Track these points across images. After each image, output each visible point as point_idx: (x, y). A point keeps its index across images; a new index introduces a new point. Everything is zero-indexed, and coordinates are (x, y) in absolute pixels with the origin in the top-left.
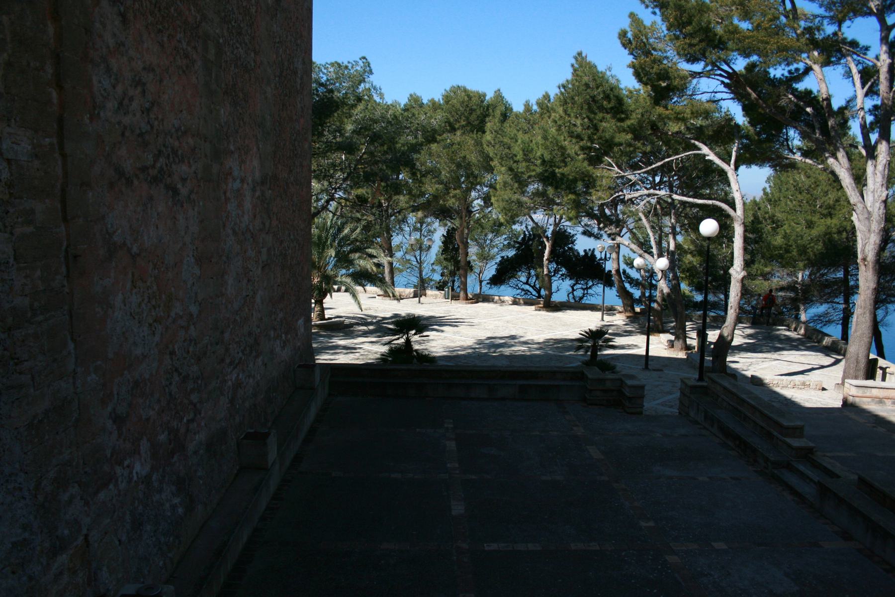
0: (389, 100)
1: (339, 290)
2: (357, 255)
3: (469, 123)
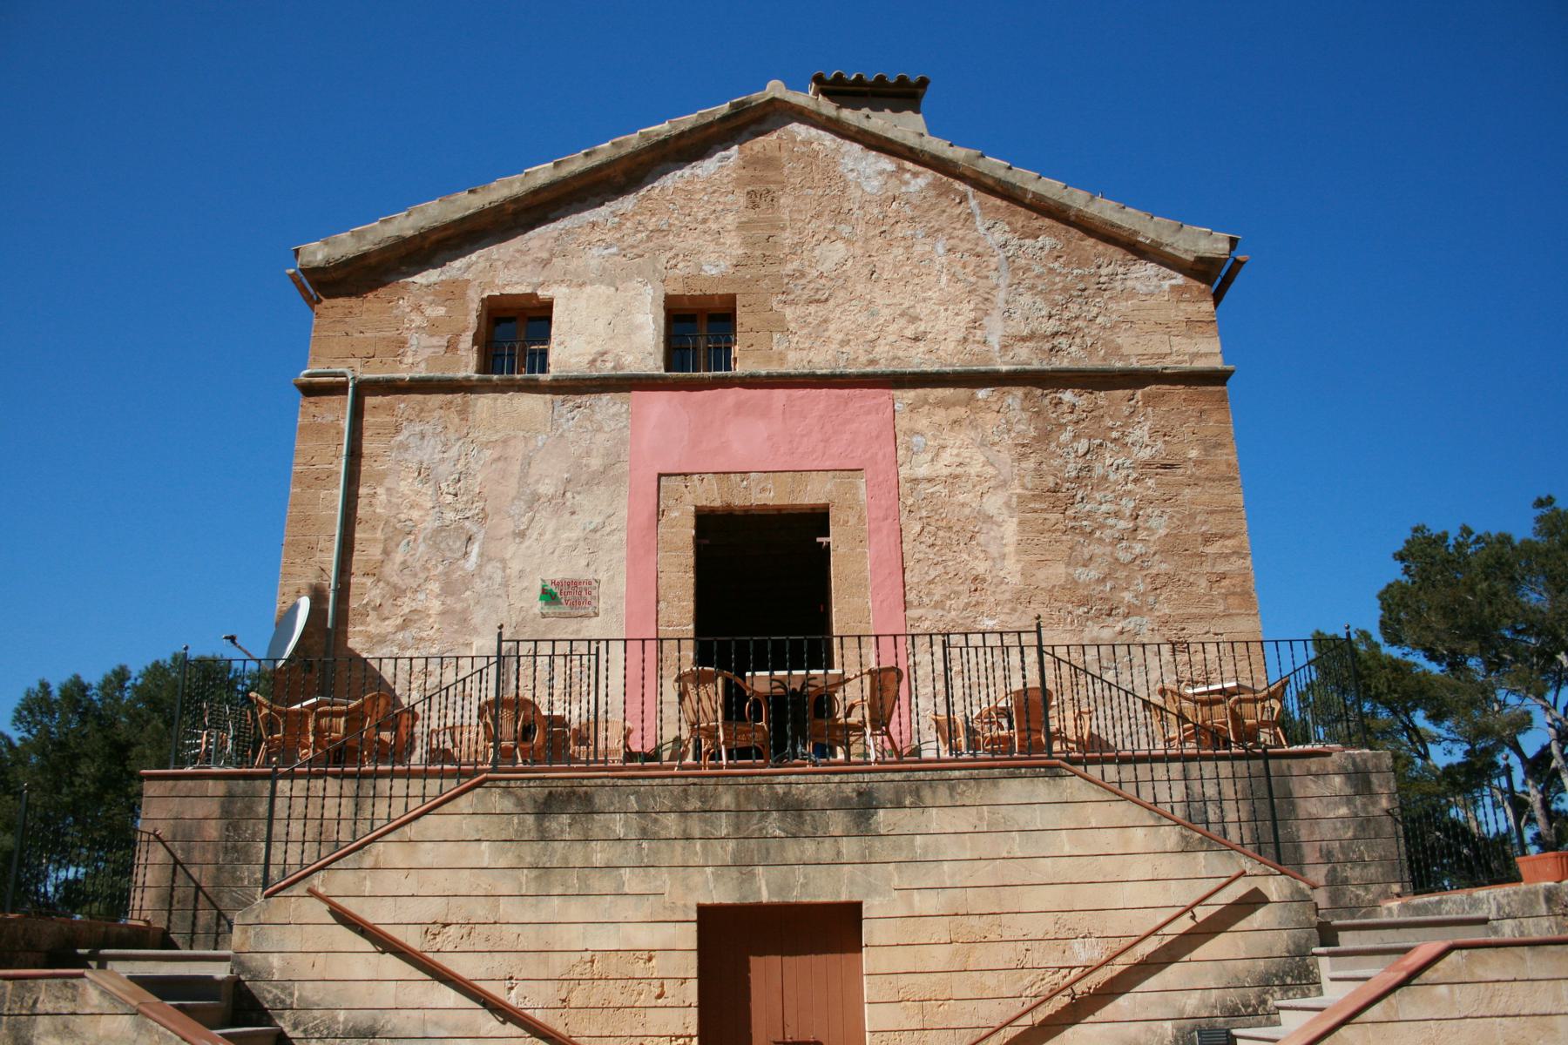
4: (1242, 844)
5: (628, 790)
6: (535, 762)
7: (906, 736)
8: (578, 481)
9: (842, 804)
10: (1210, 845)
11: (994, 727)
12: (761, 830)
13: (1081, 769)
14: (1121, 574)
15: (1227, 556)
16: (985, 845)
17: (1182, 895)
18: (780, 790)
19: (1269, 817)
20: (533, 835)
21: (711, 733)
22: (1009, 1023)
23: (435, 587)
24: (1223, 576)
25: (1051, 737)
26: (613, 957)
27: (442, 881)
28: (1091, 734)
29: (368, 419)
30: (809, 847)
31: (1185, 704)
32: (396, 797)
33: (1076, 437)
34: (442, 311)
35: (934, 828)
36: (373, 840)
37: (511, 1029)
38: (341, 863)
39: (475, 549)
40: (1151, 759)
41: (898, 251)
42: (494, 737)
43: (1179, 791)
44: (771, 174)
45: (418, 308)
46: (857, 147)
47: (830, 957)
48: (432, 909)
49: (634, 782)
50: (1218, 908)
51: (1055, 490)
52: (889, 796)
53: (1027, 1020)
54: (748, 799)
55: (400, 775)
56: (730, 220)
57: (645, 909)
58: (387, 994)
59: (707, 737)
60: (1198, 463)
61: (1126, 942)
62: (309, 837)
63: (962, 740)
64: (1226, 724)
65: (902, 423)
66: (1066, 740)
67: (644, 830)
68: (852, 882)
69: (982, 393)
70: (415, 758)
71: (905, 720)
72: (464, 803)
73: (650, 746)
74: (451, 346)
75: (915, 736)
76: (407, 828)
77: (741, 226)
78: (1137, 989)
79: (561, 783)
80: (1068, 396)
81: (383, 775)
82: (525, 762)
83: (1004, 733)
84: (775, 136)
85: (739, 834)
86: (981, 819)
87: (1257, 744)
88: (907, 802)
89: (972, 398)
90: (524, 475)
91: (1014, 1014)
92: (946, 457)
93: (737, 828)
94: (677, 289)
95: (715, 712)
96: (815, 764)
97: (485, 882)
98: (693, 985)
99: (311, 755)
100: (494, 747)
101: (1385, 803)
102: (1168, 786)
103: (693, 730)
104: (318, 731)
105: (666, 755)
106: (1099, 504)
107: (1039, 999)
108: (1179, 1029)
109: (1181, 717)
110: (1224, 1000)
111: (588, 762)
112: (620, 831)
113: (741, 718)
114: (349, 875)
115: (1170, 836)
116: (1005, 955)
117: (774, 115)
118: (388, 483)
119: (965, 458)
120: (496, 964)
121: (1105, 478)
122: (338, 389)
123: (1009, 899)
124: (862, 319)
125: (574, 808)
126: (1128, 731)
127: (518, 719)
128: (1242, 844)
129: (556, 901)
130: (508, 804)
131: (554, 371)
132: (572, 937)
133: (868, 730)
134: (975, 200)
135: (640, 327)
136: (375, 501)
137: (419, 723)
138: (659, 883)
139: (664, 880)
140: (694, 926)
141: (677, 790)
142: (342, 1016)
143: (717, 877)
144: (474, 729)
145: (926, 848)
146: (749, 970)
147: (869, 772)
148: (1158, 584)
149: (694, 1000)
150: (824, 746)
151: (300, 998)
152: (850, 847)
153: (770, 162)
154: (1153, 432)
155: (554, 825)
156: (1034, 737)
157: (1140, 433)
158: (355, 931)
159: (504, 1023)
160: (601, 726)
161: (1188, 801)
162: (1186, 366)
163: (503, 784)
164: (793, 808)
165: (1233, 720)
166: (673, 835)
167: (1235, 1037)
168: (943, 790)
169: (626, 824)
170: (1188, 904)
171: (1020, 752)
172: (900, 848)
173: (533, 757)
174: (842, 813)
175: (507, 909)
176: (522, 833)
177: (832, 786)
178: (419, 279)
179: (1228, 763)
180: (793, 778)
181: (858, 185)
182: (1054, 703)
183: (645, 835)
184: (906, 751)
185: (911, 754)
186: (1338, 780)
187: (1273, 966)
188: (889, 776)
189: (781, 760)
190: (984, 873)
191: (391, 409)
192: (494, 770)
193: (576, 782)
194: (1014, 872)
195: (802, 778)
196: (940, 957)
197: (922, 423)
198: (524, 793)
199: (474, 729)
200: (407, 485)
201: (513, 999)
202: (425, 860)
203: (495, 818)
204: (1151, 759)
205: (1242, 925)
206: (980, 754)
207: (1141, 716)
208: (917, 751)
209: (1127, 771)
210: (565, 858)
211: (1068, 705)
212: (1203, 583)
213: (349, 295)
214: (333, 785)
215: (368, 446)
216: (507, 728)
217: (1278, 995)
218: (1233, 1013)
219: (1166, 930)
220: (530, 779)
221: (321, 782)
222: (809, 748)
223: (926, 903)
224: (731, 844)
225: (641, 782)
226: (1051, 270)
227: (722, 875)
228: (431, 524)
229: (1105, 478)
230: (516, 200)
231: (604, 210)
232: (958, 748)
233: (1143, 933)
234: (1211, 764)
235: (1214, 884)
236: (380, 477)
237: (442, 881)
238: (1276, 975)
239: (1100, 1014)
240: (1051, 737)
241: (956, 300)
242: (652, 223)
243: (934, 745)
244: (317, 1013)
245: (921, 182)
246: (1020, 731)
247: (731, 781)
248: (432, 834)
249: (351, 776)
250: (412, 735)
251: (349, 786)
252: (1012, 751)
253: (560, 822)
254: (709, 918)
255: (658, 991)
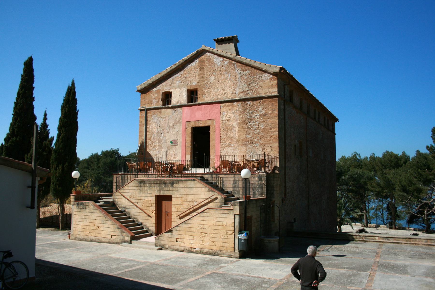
0: (363, 157)
1: (347, 224)
2: (352, 212)
3: (391, 166)
8: (176, 123)
9: (170, 183)
14: (255, 136)
15: (274, 132)
16: (186, 189)
23: (157, 141)
24: (273, 136)
29: (148, 115)
33: (250, 111)
34: (157, 95)
39: (162, 135)
41: (222, 77)
44: (203, 64)
45: (154, 95)
46: (217, 56)
48: (130, 194)
51: (245, 121)
56: (197, 74)
58: (126, 204)
60: (271, 114)
65: (222, 110)
69: (234, 103)
74: (158, 101)
77: (199, 75)
80: (249, 103)
84: (204, 56)
89: (233, 105)
90: (168, 123)
92: (228, 116)
94: (189, 88)
101: (263, 182)
106: (252, 123)
116: (187, 203)
117: (203, 52)
118: (151, 125)
119: (231, 116)
121: (254, 118)
122: (143, 110)
124: (216, 91)
131: (172, 105)
132: (143, 198)
134: (236, 64)
135: (184, 96)
136: (150, 128)
139: (152, 192)
148: (261, 137)
152: (171, 189)
153: (203, 62)
154: (263, 108)
157: (261, 109)
162: (270, 95)
175: (137, 195)
178: (154, 90)
181: (217, 64)
183: (150, 186)
186: (257, 178)
190: (185, 193)
191: (151, 113)
196: (180, 203)
197: (225, 110)
200: (153, 125)
201: (137, 205)
212: (269, 137)
213: (145, 93)
215: (148, 119)
223: (179, 196)
226: (248, 78)
228: (156, 131)
229: (254, 118)
230: (165, 75)
231: (179, 74)
236: (150, 124)
237: (131, 191)
241: (231, 86)
242: (185, 76)
245: (227, 62)
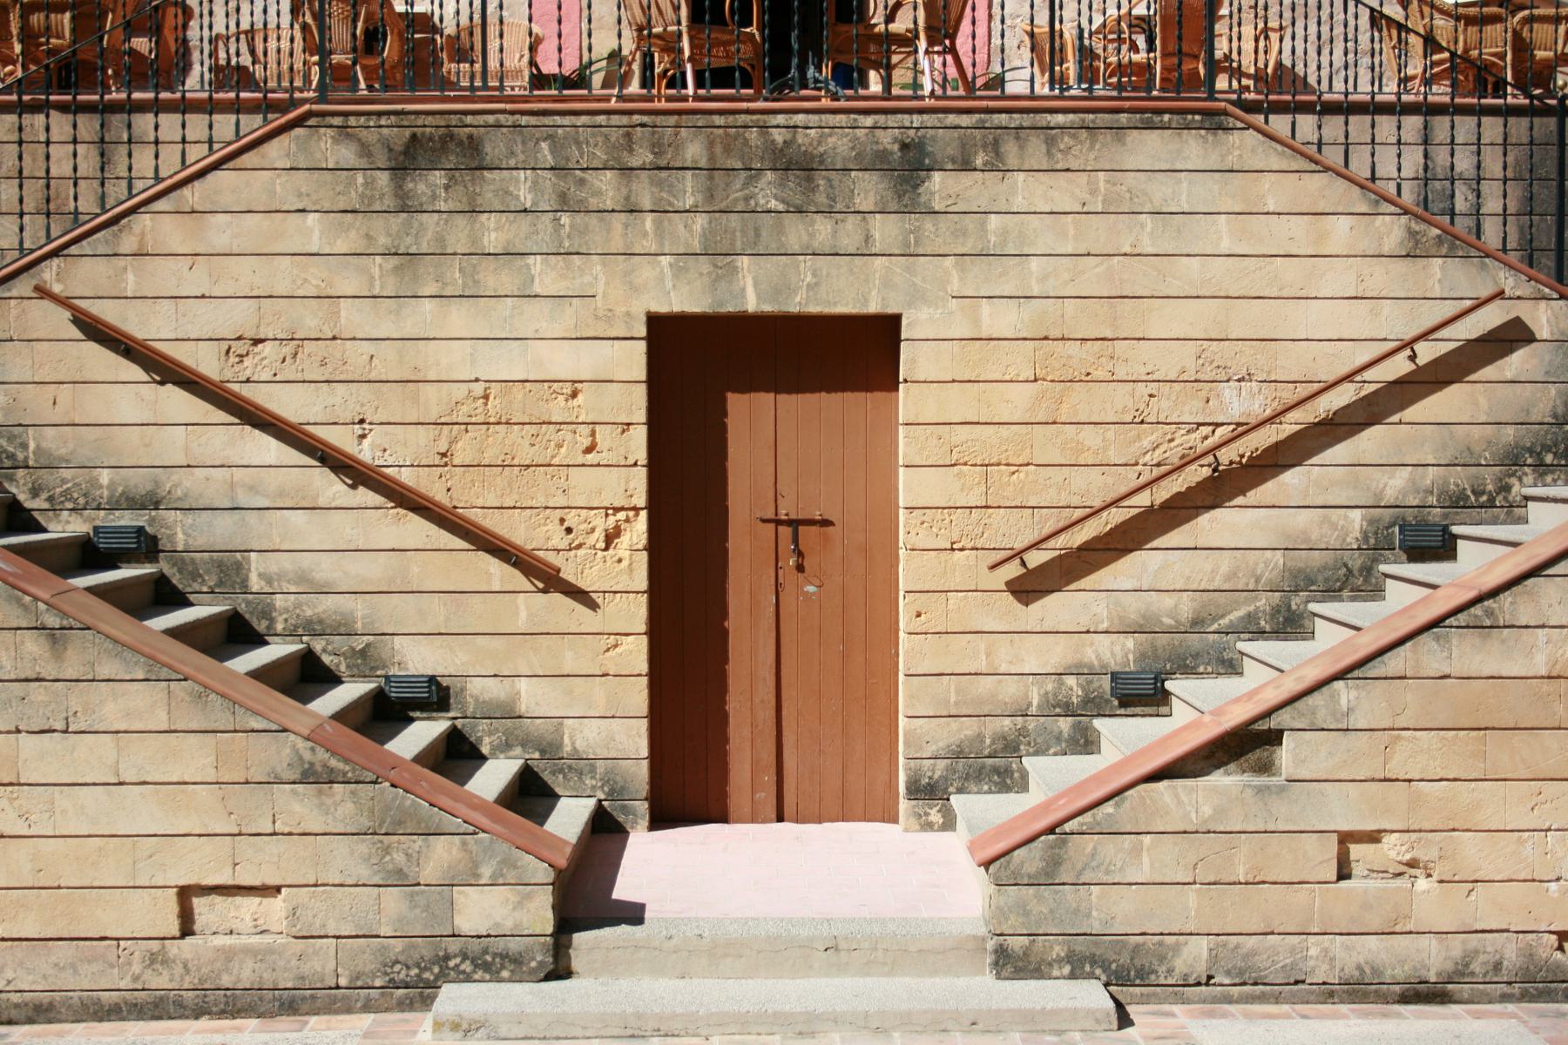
4: (1504, 250)
5: (538, 133)
6: (386, 88)
7: (981, 57)
9: (876, 162)
10: (1452, 247)
11: (1125, 48)
12: (747, 199)
13: (1259, 119)
16: (1098, 232)
17: (1399, 322)
18: (779, 136)
19: (1553, 208)
20: (389, 202)
21: (670, 44)
22: (1115, 503)
25: (1214, 67)
26: (518, 392)
27: (247, 276)
28: (1279, 65)
30: (823, 228)
31: (1440, 22)
32: (166, 141)
35: (1019, 203)
36: (133, 210)
37: (365, 496)
38: (85, 246)
40: (1374, 108)
42: (318, 46)
43: (1413, 160)
47: (848, 395)
48: (236, 318)
49: (547, 120)
50: (1452, 345)
52: (950, 151)
53: (1143, 499)
54: (727, 150)
55: (170, 107)
57: (568, 318)
58: (172, 445)
59: (663, 50)
61: (1303, 391)
62: (29, 206)
63: (1071, 67)
64: (1502, 56)
66: (1238, 73)
67: (563, 197)
68: (887, 283)
70: (192, 81)
71: (981, 30)
72: (275, 151)
73: (571, 66)
75: (996, 60)
76: (186, 191)
78: (1314, 460)
79: (430, 120)
81: (142, 107)
82: (370, 88)
83: (1140, 57)
85: (713, 206)
86: (1093, 192)
87: (1550, 93)
88: (979, 162)
91: (1123, 490)
93: (710, 195)
95: (677, 9)
96: (835, 98)
97: (315, 276)
98: (640, 435)
99: (19, 74)
100: (320, 64)
102: (1395, 153)
103: (640, 38)
104: (27, 35)
105: (597, 80)
107: (1163, 469)
108: (1371, 522)
109: (1431, 43)
110: (1446, 483)
111: (472, 88)
112: (526, 197)
113: (718, 19)
114: (101, 266)
115: (1391, 230)
116: (1120, 400)
120: (338, 400)
123: (1129, 318)
125: (451, 160)
126: (1338, 60)
127: (355, 21)
128: (1504, 250)
129: (428, 304)
130: (346, 154)
132: (452, 360)
133: (922, 44)
137: (194, 24)
138: (588, 279)
139: (595, 275)
140: (642, 346)
141: (615, 135)
142: (105, 477)
143: (678, 271)
144: (286, 34)
145: (1004, 233)
146: (725, 414)
147: (921, 111)
149: (641, 455)
150: (850, 69)
151: (39, 451)
152: (885, 230)
155: (421, 187)
156: (1187, 66)
158: (117, 352)
159: (353, 487)
160: (493, 31)
161: (1426, 177)
163: (337, 121)
164: (799, 166)
165: (1515, 50)
166: (609, 205)
167: (1455, 537)
168: (1036, 144)
169: (535, 187)
170: (1408, 337)
171: (1162, 89)
172: (964, 233)
173: (384, 80)
174: (875, 176)
175: (352, 317)
176: (372, 199)
177: (860, 133)
179: (1500, 121)
180: (800, 119)
182: (1224, 11)
183: (565, 204)
184: (979, 82)
185: (986, 86)
187: (1527, 436)
188: (952, 119)
189: (780, 89)
190: (1093, 278)
192: (323, 99)
193: (454, 119)
194: (1139, 277)
195: (813, 119)
196: (1017, 401)
198: (371, 136)
199: (286, 34)
201: (366, 453)
202: (221, 242)
203: (327, 175)
204: (1374, 108)
205: (1488, 372)
206: (1099, 89)
207: (1364, 39)
208: (1000, 81)
209: (1333, 126)
210: (440, 239)
211: (1248, 16)
214: (60, 124)
216: (340, 33)
217: (1529, 479)
218: (1457, 502)
219: (1368, 375)
220: (380, 114)
221: (40, 119)
222: (827, 71)
223: (1001, 319)
224: (700, 221)
225: (558, 120)
227: (685, 269)
232: (1063, 80)
233: (1331, 378)
234: (1471, 121)
235: (1450, 309)
237: (247, 276)
238: (1531, 451)
239: (1253, 496)
240: (1214, 67)
243: (1026, 74)
244: (66, 474)
246: (1165, 55)
247: (701, 120)
248: (227, 201)
249: (89, 108)
250: (185, 41)
251: (88, 125)
252: (1150, 86)
253: (429, 184)
254: (669, 338)
255: (587, 442)
